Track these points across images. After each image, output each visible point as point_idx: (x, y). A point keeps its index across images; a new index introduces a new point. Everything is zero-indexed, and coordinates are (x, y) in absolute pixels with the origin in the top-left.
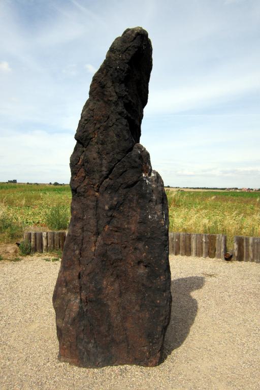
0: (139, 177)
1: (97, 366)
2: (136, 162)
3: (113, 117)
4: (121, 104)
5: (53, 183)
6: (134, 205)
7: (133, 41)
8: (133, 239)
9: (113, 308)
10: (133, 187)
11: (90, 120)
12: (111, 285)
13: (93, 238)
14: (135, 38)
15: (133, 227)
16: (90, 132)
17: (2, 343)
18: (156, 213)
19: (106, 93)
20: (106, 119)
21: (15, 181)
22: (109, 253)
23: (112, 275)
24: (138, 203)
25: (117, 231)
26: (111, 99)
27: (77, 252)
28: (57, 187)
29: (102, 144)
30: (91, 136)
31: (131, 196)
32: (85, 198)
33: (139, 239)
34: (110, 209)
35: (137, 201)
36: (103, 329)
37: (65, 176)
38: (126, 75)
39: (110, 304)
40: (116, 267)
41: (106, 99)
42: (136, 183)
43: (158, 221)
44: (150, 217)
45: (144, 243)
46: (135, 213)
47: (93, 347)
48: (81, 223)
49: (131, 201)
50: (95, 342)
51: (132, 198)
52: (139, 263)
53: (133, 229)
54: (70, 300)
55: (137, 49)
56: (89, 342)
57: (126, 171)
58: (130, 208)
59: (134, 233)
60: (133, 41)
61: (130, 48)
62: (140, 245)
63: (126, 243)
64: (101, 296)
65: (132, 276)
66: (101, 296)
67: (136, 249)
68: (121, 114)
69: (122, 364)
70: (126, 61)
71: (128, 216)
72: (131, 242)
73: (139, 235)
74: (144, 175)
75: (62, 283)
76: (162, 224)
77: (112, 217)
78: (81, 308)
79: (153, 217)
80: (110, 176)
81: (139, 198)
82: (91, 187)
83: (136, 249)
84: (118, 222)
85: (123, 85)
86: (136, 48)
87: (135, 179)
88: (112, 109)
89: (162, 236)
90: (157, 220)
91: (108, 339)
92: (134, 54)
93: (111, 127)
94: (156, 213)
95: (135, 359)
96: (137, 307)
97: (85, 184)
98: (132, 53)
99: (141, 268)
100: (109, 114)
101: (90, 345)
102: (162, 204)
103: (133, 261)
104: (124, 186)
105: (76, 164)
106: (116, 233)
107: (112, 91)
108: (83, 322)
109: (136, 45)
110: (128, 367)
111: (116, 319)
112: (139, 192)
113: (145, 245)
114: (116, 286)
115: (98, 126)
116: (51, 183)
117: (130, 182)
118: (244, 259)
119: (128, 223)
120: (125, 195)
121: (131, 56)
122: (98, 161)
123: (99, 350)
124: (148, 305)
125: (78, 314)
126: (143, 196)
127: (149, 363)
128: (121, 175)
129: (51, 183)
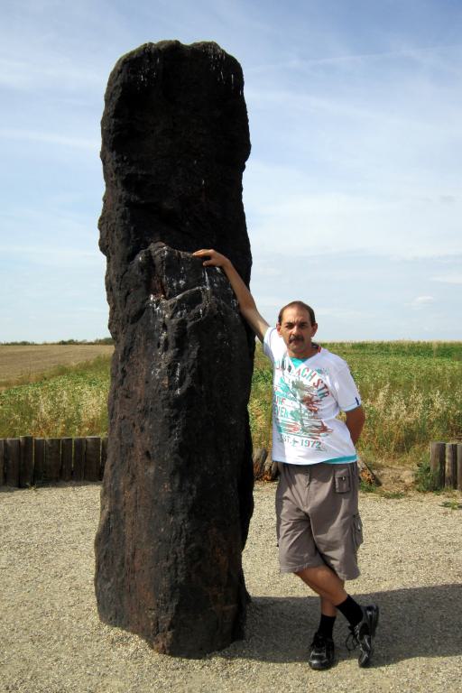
0: (143, 302)
42: (140, 313)
53: (139, 393)
55: (121, 90)
58: (138, 356)
76: (163, 385)
87: (138, 306)
90: (158, 377)
107: (112, 156)
120: (132, 335)
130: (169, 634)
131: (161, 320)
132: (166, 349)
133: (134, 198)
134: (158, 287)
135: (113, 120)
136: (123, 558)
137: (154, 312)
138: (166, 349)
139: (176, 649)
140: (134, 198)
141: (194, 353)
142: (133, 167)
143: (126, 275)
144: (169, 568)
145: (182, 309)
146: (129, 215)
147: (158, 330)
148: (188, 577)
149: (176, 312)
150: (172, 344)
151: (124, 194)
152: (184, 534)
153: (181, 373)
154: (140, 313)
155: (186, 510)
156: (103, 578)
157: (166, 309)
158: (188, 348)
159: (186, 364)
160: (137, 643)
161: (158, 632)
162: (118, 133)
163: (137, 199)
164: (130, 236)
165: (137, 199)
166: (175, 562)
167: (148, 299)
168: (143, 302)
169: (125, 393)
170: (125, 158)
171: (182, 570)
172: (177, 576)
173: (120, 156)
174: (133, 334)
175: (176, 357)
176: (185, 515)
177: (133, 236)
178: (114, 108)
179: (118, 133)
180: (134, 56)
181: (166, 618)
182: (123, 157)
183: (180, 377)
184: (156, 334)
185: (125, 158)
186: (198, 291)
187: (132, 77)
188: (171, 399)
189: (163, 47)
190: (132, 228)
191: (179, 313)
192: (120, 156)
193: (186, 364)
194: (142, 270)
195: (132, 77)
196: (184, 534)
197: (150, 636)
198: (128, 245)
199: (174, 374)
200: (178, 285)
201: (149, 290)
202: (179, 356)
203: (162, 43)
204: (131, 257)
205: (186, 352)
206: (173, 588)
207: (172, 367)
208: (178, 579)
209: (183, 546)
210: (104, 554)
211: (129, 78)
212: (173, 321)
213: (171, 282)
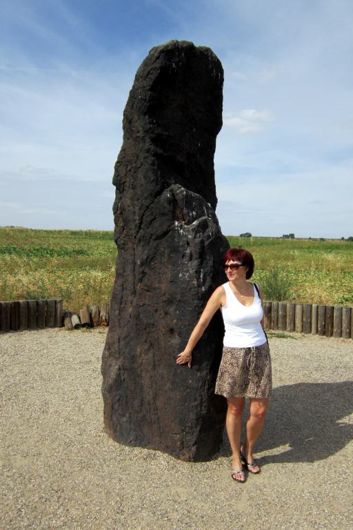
0: (169, 226)
1: (130, 444)
2: (165, 208)
3: (142, 155)
4: (148, 140)
5: (346, 238)
6: (165, 260)
7: (155, 62)
8: (165, 302)
9: (146, 381)
10: (164, 239)
11: (122, 162)
12: (146, 354)
13: (130, 297)
14: (158, 58)
15: (163, 287)
16: (122, 175)
17: (1, 391)
18: (188, 271)
19: (133, 129)
20: (136, 159)
21: (292, 236)
22: (141, 316)
23: (146, 342)
24: (170, 258)
25: (148, 291)
26: (138, 135)
27: (117, 312)
28: (104, 236)
29: (133, 189)
30: (123, 180)
31: (162, 249)
32: (125, 251)
33: (170, 302)
34: (142, 264)
35: (169, 255)
36: (137, 403)
37: (107, 223)
38: (148, 104)
39: (143, 375)
40: (149, 332)
41: (134, 136)
42: (166, 233)
43: (189, 281)
44: (180, 275)
45: (174, 307)
46: (166, 270)
47: (127, 422)
48: (122, 280)
49: (162, 255)
50: (130, 417)
51: (163, 252)
52: (172, 331)
53: (163, 288)
54: (111, 365)
55: (159, 72)
56: (123, 415)
57: (154, 219)
58: (161, 263)
59: (164, 294)
60: (155, 62)
61: (151, 72)
62: (171, 309)
63: (156, 305)
64: (136, 366)
65: (163, 346)
66: (136, 366)
67: (166, 313)
68: (148, 151)
69: (155, 449)
70: (148, 88)
71: (159, 273)
72: (162, 304)
73: (169, 297)
74: (176, 224)
75: (109, 346)
76: (193, 284)
77: (144, 273)
78: (119, 375)
79: (183, 275)
80: (142, 226)
81: (171, 252)
82: (129, 239)
83: (166, 313)
84: (149, 280)
85: (147, 117)
86: (158, 69)
87: (165, 228)
88: (141, 146)
89: (193, 300)
90: (188, 279)
91: (140, 415)
92: (157, 78)
93: (139, 168)
94: (188, 271)
95: (167, 447)
96: (169, 385)
97: (123, 236)
98: (153, 77)
99: (175, 338)
100: (138, 152)
101: (125, 419)
102: (200, 260)
103: (163, 327)
104: (154, 237)
105: (119, 211)
106: (148, 293)
107: (140, 124)
108: (120, 391)
109: (157, 65)
110: (159, 453)
111: (149, 396)
112: (171, 245)
113: (176, 310)
114: (151, 355)
115: (129, 168)
116: (343, 238)
117: (159, 232)
118: (24, 320)
119: (160, 282)
120: (156, 248)
121: (152, 81)
122: (131, 208)
123: (132, 426)
124: (180, 385)
125: (116, 382)
126: (175, 250)
127: (181, 456)
128: (151, 223)
129: (343, 238)
130: (194, 449)
131: (185, 239)
132: (191, 259)
133: (160, 151)
134: (180, 216)
135: (149, 93)
136: (142, 400)
137: (179, 234)
138: (191, 259)
139: (197, 458)
140: (160, 151)
141: (211, 263)
142: (160, 129)
143: (152, 205)
144: (196, 407)
145: (199, 232)
146: (156, 163)
147: (183, 246)
148: (209, 411)
149: (196, 234)
150: (195, 256)
151: (153, 147)
152: (207, 383)
153: (204, 276)
154: (166, 233)
155: (208, 367)
156: (119, 414)
157: (188, 231)
158: (206, 259)
159: (206, 269)
160: (163, 459)
161: (183, 448)
162: (152, 102)
163: (162, 152)
164: (157, 179)
165: (162, 152)
166: (201, 403)
167: (174, 224)
168: (169, 226)
169: (147, 288)
170: (155, 121)
171: (205, 406)
172: (201, 410)
173: (151, 119)
174: (156, 248)
175: (200, 265)
176: (208, 371)
177: (159, 179)
178: (151, 83)
179: (152, 102)
180: (169, 48)
181: (191, 439)
182: (153, 121)
183: (203, 279)
184: (181, 249)
185: (155, 121)
186: (205, 220)
187: (168, 63)
188: (200, 295)
189: (185, 45)
190: (159, 173)
191: (198, 235)
192: (151, 119)
193: (206, 269)
194: (170, 204)
195: (168, 63)
196: (207, 383)
197: (175, 451)
198: (157, 185)
199: (199, 278)
200: (193, 215)
201: (175, 218)
202: (201, 265)
203: (184, 42)
204: (159, 193)
205: (205, 262)
206: (197, 420)
207: (198, 272)
208: (202, 412)
209: (206, 391)
210: (118, 398)
211: (166, 63)
212: (196, 240)
213: (189, 213)
